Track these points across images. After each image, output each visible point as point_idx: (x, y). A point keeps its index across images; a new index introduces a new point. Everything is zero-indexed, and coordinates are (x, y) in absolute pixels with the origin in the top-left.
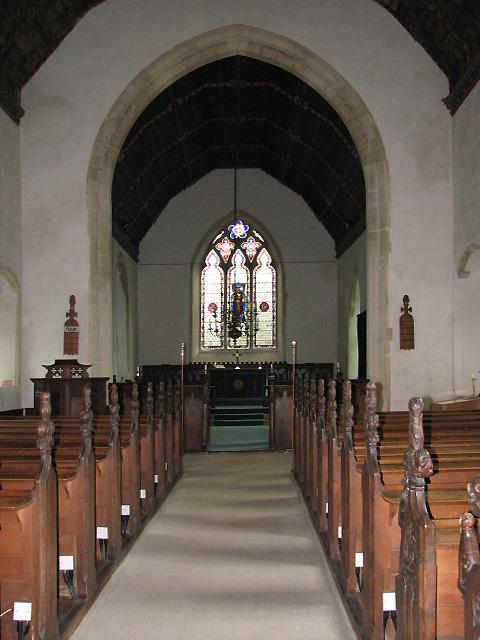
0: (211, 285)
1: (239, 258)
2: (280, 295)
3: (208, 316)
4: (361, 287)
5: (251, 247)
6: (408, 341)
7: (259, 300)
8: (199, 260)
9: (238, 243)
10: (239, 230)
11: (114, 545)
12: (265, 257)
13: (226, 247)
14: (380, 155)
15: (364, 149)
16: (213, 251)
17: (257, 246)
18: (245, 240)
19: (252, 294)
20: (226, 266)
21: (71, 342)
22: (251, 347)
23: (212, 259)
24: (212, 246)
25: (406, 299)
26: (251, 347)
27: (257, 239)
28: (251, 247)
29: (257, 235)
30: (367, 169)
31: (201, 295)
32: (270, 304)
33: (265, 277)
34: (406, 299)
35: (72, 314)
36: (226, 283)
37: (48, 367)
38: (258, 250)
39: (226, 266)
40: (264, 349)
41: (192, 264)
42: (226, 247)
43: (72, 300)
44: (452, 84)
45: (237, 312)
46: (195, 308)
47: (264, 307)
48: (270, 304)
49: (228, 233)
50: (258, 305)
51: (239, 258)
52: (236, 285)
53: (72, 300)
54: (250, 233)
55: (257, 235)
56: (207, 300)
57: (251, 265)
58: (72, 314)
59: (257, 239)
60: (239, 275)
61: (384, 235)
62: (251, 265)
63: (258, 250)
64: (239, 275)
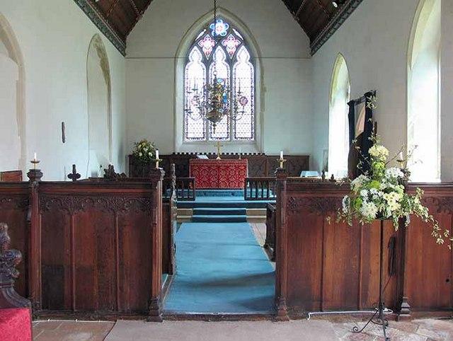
1: (220, 55)
9: (219, 40)
12: (244, 55)
17: (237, 44)
20: (208, 61)
22: (207, 139)
23: (195, 55)
38: (238, 47)
39: (208, 61)
54: (230, 31)
57: (231, 61)
60: (221, 70)
62: (231, 61)
63: (238, 47)
64: (221, 70)
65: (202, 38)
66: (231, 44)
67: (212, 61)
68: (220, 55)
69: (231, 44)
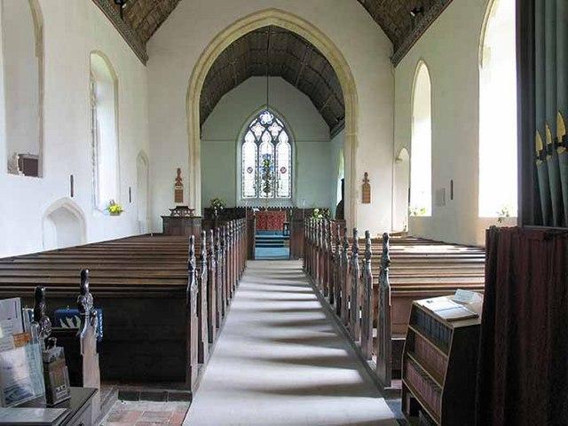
0: (248, 154)
1: (266, 137)
2: (294, 163)
3: (246, 175)
4: (176, 394)
5: (275, 129)
6: (366, 199)
7: (280, 165)
8: (240, 139)
9: (267, 126)
11: (19, 415)
12: (284, 137)
13: (258, 129)
14: (352, 91)
15: (345, 87)
16: (250, 132)
18: (271, 125)
20: (258, 142)
21: (179, 196)
23: (249, 137)
24: (249, 129)
25: (366, 174)
27: (279, 125)
28: (275, 129)
29: (279, 122)
30: (347, 98)
31: (242, 161)
32: (287, 169)
33: (284, 150)
34: (366, 174)
35: (179, 179)
37: (172, 210)
38: (280, 132)
39: (258, 142)
40: (282, 199)
41: (237, 140)
42: (258, 129)
43: (179, 171)
45: (267, 171)
46: (239, 160)
48: (287, 169)
49: (259, 120)
50: (279, 169)
51: (266, 137)
52: (265, 159)
53: (179, 171)
54: (274, 120)
55: (279, 122)
56: (246, 165)
57: (275, 142)
58: (179, 179)
59: (279, 125)
60: (267, 148)
61: (354, 137)
62: (275, 142)
63: (280, 132)
64: (267, 148)
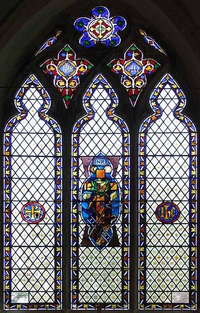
1: (100, 99)
3: (21, 233)
7: (156, 192)
9: (101, 58)
10: (101, 28)
12: (169, 98)
17: (149, 67)
19: (136, 180)
20: (67, 113)
22: (66, 305)
23: (33, 98)
26: (66, 305)
32: (184, 208)
36: (67, 157)
38: (152, 79)
39: (67, 113)
44: (61, 122)
47: (168, 213)
54: (129, 36)
57: (134, 112)
60: (100, 136)
62: (134, 112)
63: (152, 79)
64: (100, 136)
65: (53, 54)
66: (133, 69)
67: (148, 111)
68: (100, 99)
69: (133, 69)
